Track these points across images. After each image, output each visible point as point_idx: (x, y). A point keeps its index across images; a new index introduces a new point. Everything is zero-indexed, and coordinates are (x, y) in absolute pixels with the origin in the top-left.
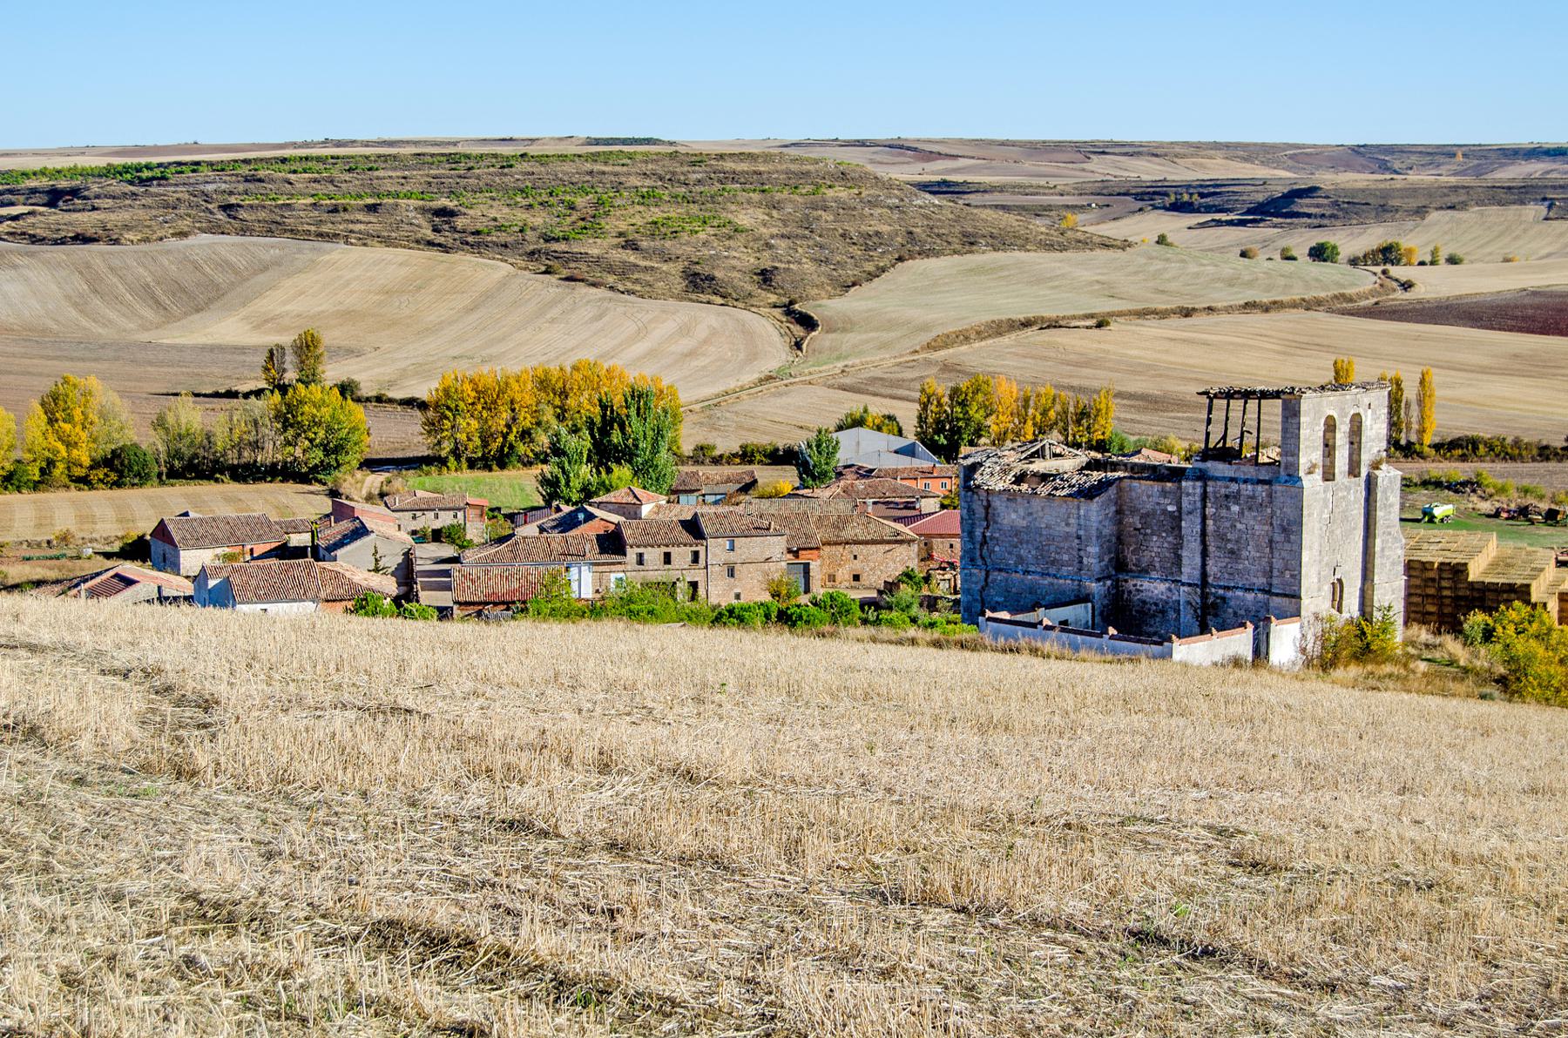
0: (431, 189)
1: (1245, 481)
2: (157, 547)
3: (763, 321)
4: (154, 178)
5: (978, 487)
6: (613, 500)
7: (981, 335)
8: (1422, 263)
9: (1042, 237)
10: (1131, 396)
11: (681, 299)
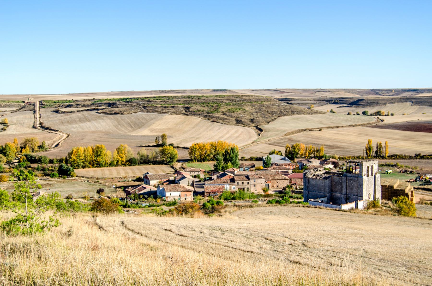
1: (353, 177)
2: (145, 179)
3: (252, 130)
5: (307, 177)
7: (296, 133)
8: (386, 115)
10: (327, 146)
11: (235, 125)
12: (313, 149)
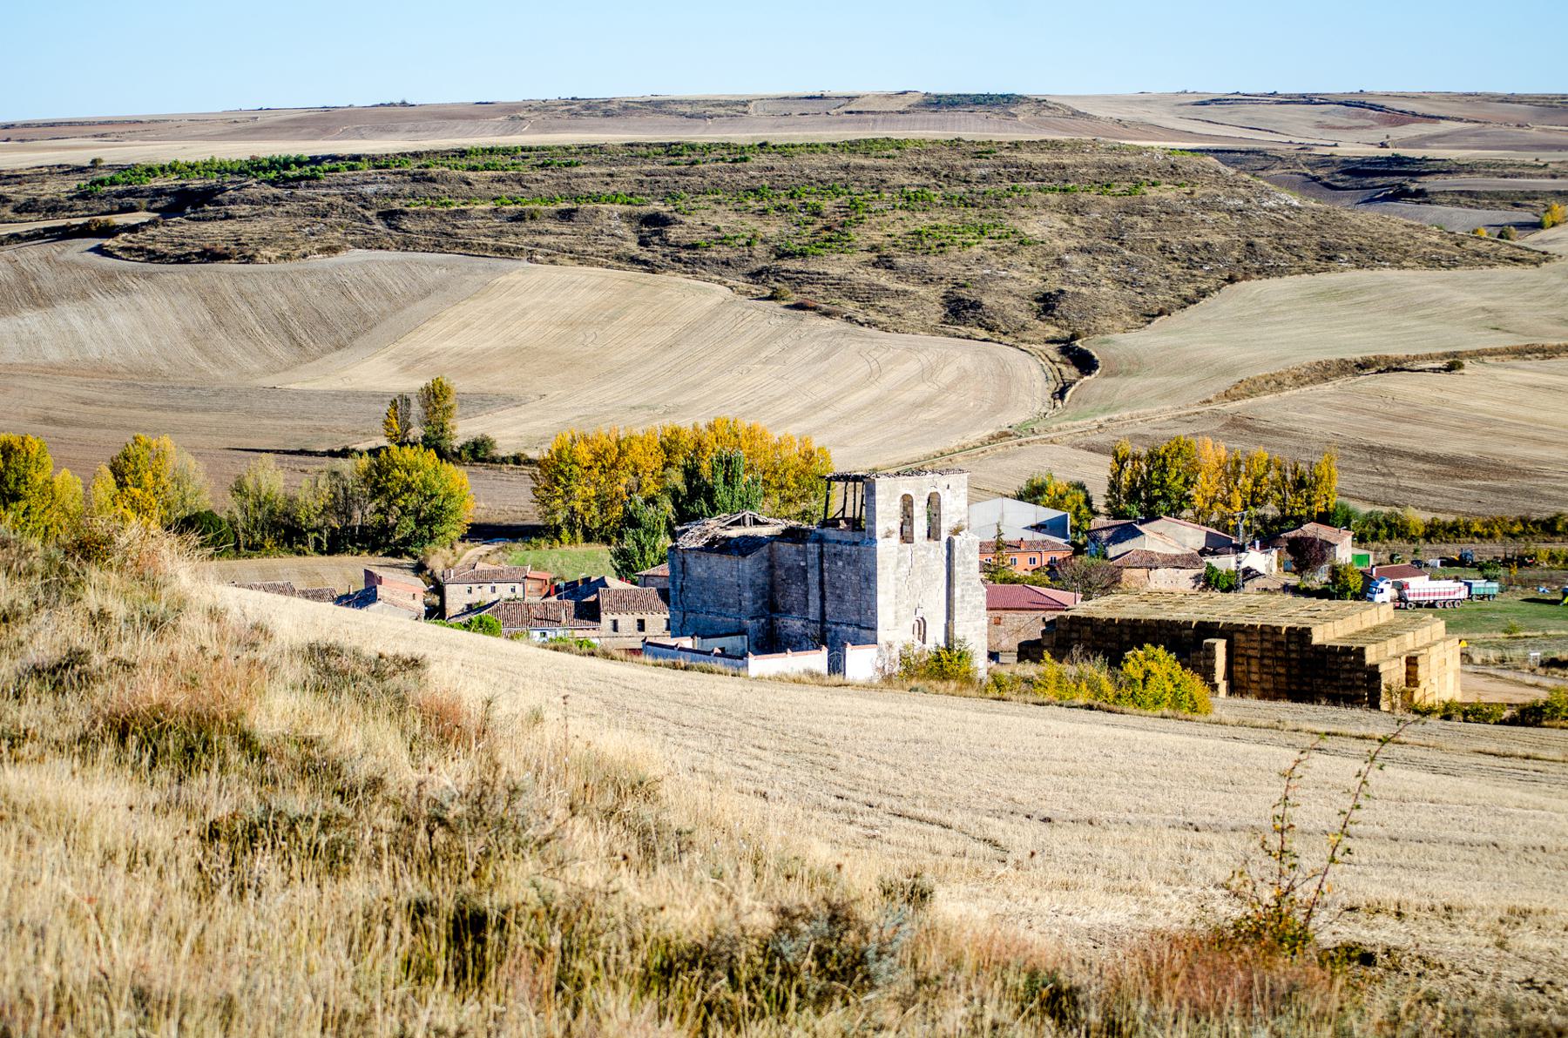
0: (643, 190)
3: (1031, 361)
4: (301, 178)
6: (660, 573)
7: (1299, 380)
9: (1428, 249)
11: (934, 331)
12: (1274, 474)
